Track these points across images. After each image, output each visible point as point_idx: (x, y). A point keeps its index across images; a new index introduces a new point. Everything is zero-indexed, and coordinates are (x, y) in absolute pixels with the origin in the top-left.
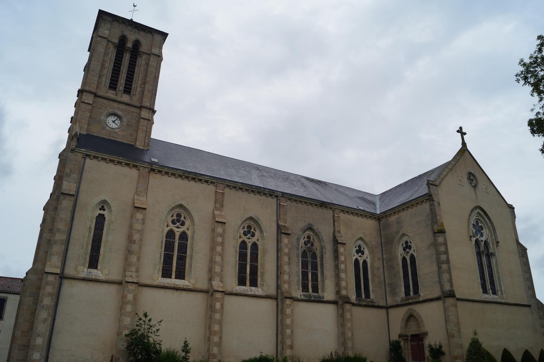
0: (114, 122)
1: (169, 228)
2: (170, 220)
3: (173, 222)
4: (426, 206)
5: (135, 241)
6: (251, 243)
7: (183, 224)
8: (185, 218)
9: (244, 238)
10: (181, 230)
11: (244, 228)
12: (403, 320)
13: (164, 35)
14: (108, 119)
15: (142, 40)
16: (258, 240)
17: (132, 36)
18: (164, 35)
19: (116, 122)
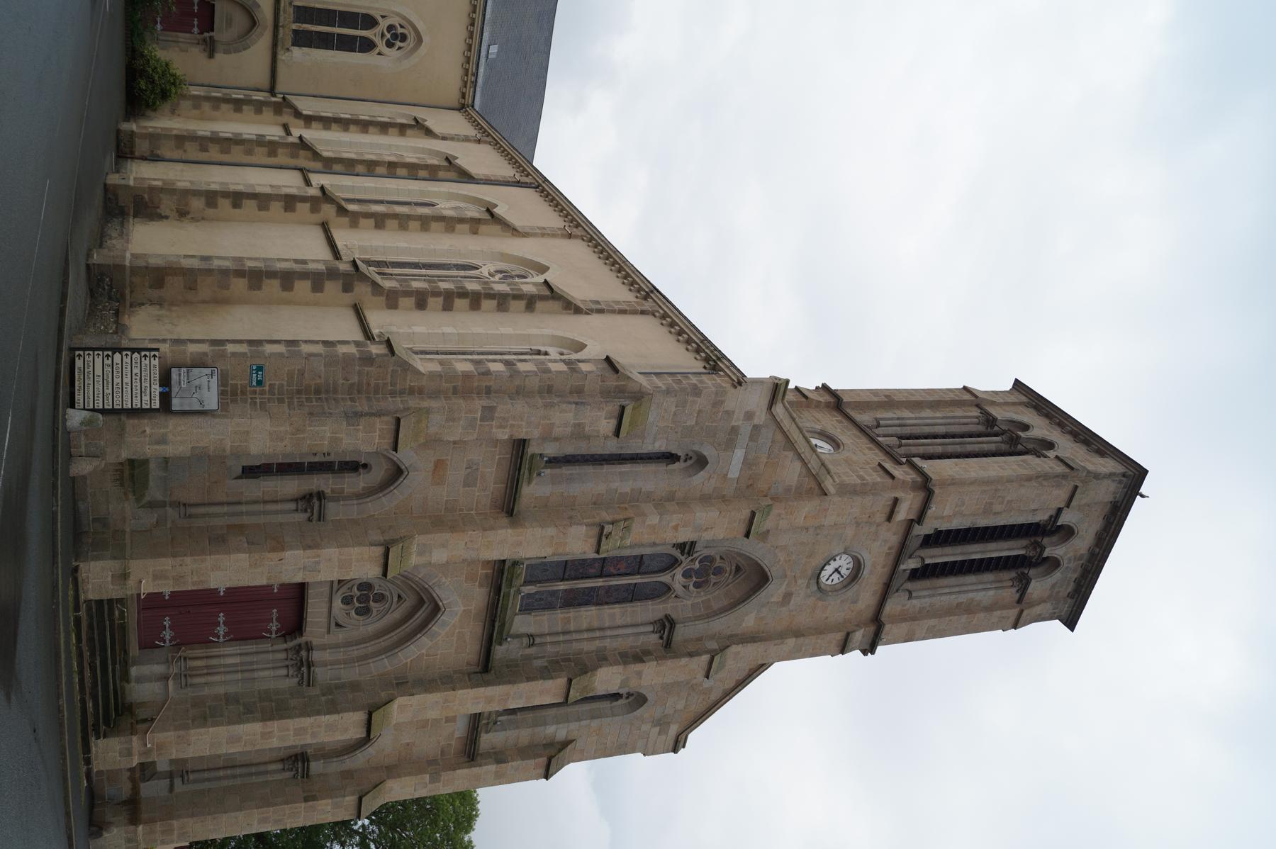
0: (837, 570)
1: (380, 20)
2: (395, 21)
3: (390, 28)
4: (453, 96)
5: (259, 288)
6: (372, 37)
7: (390, 45)
8: (399, 48)
9: (383, 24)
10: (377, 40)
11: (402, 27)
12: (240, 260)
13: (1071, 623)
14: (850, 559)
15: (1057, 575)
16: (379, 54)
17: (1068, 552)
18: (1071, 623)
19: (836, 576)
